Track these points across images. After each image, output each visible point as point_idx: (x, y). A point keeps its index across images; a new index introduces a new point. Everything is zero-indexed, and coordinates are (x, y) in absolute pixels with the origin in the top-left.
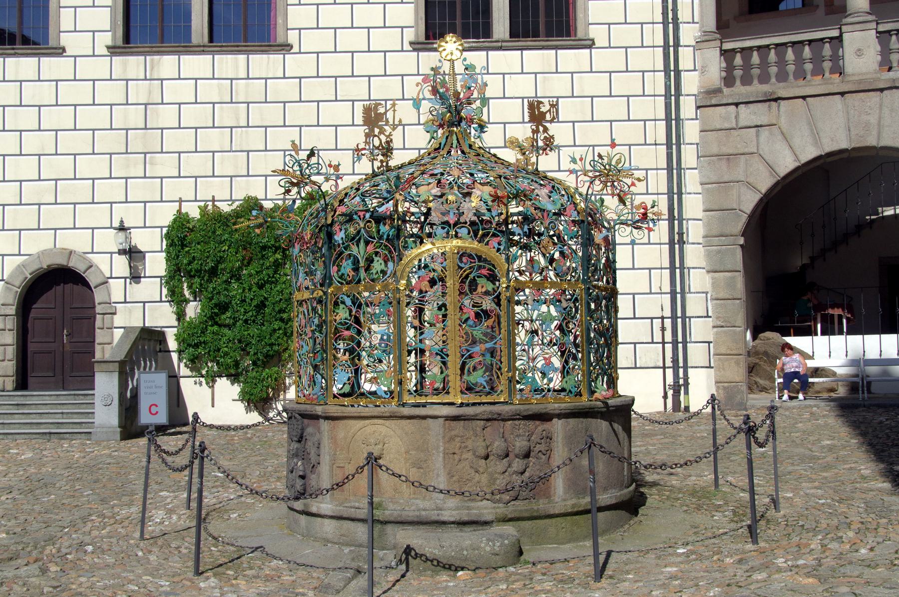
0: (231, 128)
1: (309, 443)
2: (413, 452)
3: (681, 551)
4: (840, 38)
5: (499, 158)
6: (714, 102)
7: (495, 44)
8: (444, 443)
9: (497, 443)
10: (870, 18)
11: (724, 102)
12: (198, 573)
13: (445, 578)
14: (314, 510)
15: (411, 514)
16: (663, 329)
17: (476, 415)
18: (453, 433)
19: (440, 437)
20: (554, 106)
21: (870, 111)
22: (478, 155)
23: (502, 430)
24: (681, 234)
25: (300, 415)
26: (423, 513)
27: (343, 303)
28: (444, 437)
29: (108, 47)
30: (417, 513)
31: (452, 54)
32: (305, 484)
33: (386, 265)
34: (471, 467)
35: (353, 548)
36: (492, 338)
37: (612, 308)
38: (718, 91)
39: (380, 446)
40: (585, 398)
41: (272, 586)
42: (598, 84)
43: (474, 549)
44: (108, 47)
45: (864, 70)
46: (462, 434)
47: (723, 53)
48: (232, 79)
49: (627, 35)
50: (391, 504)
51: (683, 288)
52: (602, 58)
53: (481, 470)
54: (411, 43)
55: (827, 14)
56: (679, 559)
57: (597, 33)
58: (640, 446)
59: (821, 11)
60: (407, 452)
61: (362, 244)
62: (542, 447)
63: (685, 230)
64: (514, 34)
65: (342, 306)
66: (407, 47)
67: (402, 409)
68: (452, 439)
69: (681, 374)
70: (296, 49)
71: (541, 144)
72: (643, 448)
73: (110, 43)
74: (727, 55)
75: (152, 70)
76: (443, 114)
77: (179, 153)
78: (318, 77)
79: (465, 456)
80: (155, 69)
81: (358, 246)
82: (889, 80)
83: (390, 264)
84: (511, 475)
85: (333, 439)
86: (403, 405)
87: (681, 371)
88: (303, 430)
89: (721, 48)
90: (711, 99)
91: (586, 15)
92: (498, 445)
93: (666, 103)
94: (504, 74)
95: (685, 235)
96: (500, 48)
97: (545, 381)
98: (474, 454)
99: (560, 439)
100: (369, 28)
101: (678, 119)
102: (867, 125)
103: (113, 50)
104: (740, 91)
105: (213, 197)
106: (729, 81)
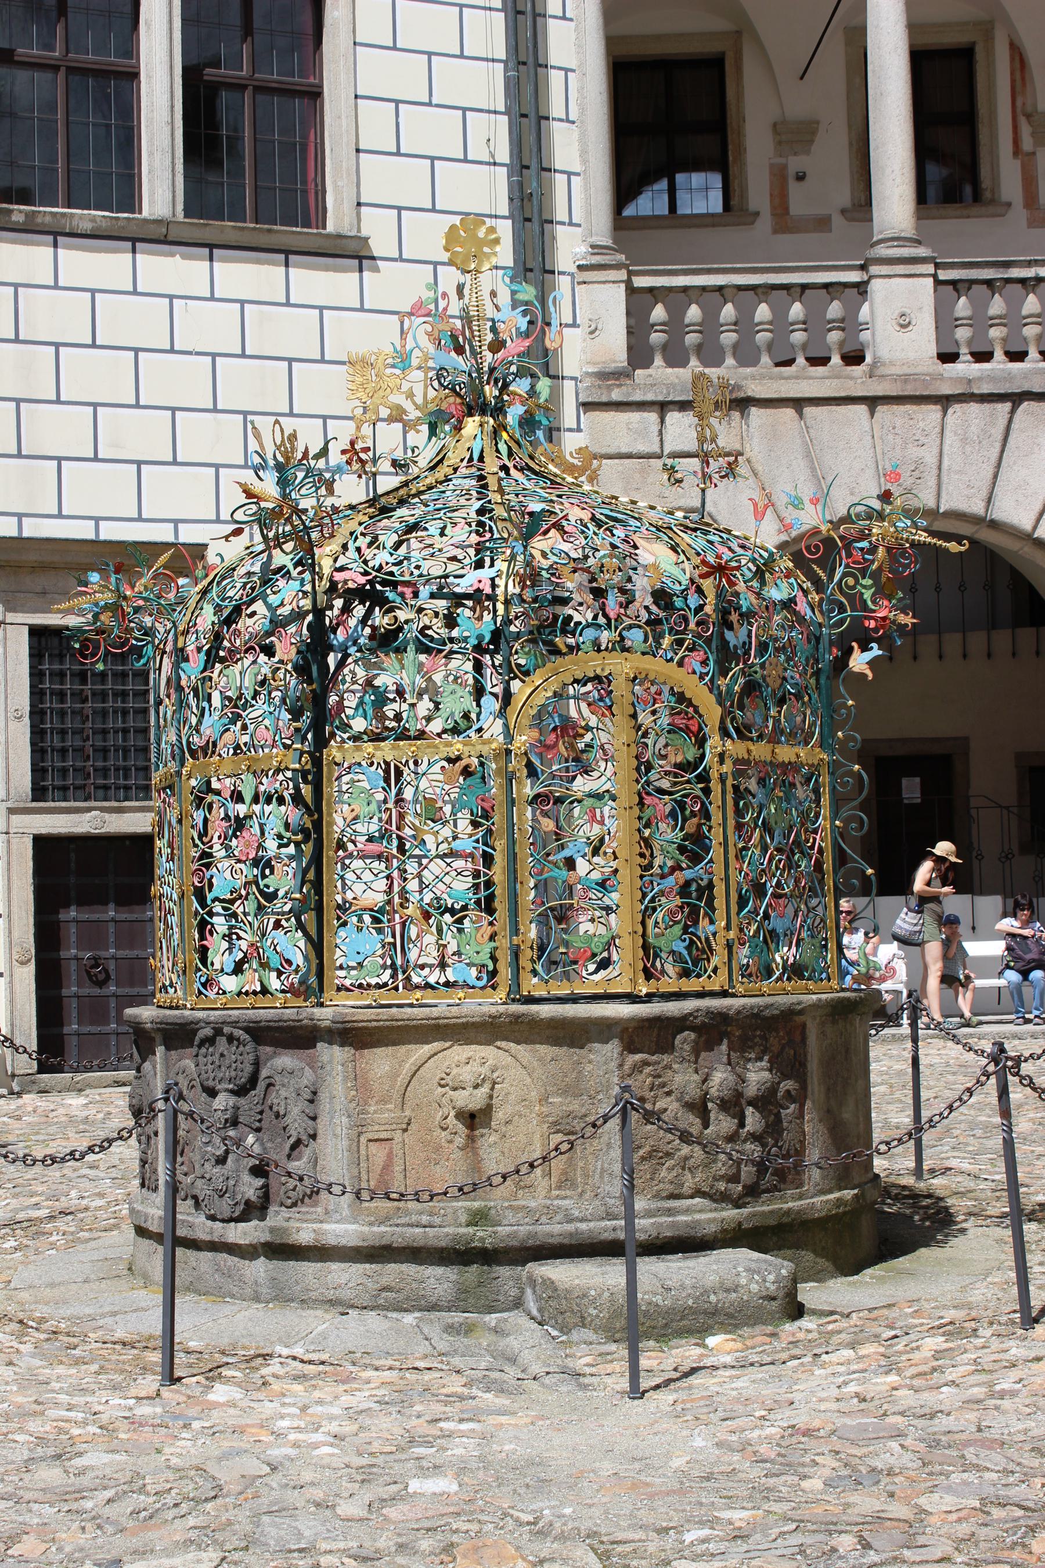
2: (557, 1100)
4: (861, 289)
6: (616, 395)
10: (922, 251)
11: (638, 397)
14: (304, 1236)
15: (557, 1229)
19: (613, 1065)
21: (923, 440)
25: (247, 1030)
26: (583, 1226)
30: (570, 1227)
32: (266, 1186)
36: (695, 859)
38: (618, 375)
39: (485, 1090)
43: (728, 1291)
45: (912, 355)
47: (631, 291)
50: (509, 1214)
55: (775, 232)
59: (765, 223)
60: (543, 1100)
64: (197, 203)
68: (638, 1068)
74: (638, 301)
82: (959, 380)
85: (359, 1082)
88: (257, 1065)
89: (628, 283)
90: (609, 388)
94: (171, 297)
96: (164, 241)
102: (918, 465)
104: (661, 377)
106: (639, 354)
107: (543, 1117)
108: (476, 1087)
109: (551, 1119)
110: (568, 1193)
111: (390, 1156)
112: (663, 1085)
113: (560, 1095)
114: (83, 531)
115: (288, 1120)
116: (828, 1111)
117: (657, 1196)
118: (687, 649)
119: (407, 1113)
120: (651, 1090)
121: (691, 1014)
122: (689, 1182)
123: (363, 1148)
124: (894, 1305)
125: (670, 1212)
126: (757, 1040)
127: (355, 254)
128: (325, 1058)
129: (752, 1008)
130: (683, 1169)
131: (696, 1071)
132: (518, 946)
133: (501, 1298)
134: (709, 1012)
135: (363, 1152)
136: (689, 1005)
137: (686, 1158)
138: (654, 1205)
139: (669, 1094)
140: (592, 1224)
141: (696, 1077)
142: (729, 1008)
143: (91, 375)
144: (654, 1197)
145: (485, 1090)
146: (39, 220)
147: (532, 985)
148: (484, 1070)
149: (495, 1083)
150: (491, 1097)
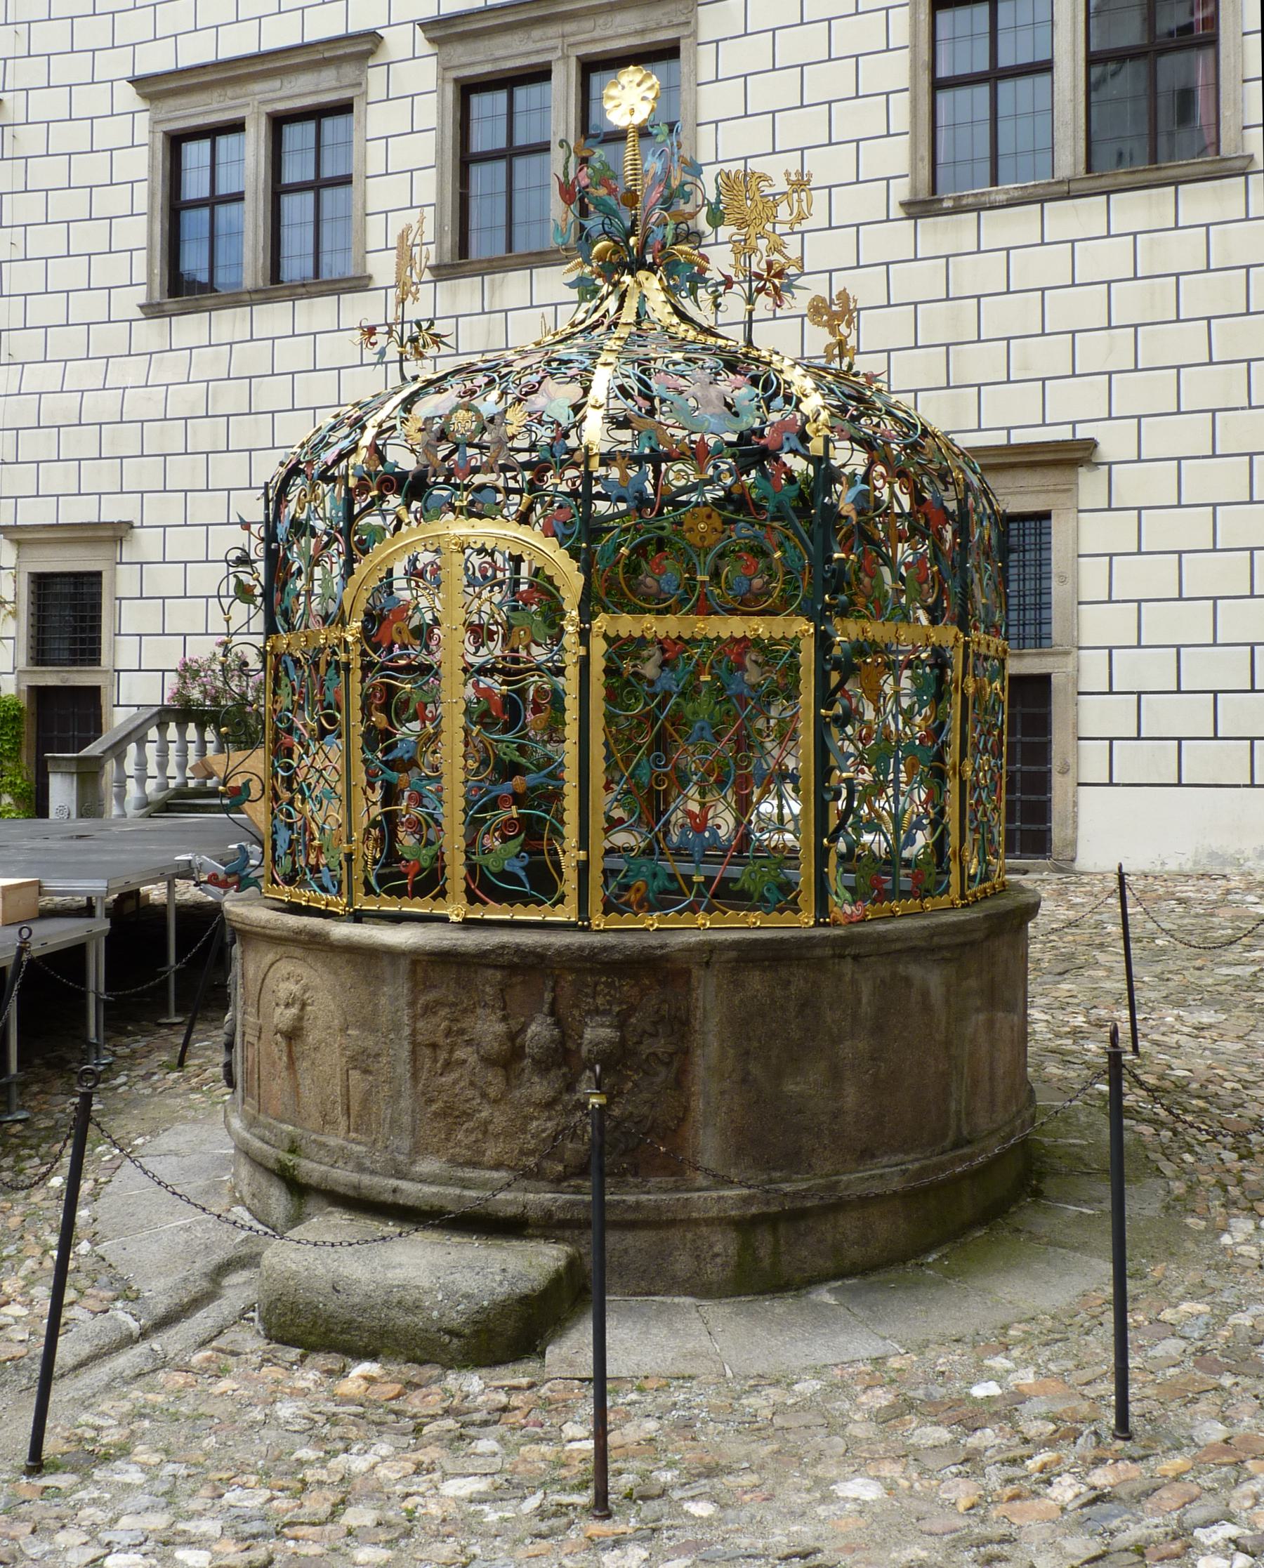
7: (1056, 188)
8: (414, 1018)
9: (533, 1028)
12: (602, 1508)
19: (403, 1002)
28: (412, 1004)
29: (141, 307)
30: (355, 1177)
39: (294, 1011)
40: (807, 918)
44: (141, 307)
46: (451, 998)
54: (902, 204)
60: (344, 1030)
62: (660, 1046)
66: (896, 212)
68: (429, 1010)
73: (143, 301)
75: (492, 296)
79: (460, 1054)
80: (497, 294)
96: (1068, 196)
99: (713, 1025)
103: (152, 310)
108: (287, 1005)
110: (363, 1138)
112: (462, 1032)
113: (358, 1028)
114: (999, 439)
116: (744, 1081)
120: (447, 1036)
121: (492, 951)
122: (492, 1151)
124: (691, 1378)
125: (465, 1184)
130: (485, 1132)
131: (504, 1019)
134: (518, 950)
137: (486, 1123)
140: (376, 1179)
142: (547, 947)
143: (1003, 315)
145: (294, 1011)
146: (964, 202)
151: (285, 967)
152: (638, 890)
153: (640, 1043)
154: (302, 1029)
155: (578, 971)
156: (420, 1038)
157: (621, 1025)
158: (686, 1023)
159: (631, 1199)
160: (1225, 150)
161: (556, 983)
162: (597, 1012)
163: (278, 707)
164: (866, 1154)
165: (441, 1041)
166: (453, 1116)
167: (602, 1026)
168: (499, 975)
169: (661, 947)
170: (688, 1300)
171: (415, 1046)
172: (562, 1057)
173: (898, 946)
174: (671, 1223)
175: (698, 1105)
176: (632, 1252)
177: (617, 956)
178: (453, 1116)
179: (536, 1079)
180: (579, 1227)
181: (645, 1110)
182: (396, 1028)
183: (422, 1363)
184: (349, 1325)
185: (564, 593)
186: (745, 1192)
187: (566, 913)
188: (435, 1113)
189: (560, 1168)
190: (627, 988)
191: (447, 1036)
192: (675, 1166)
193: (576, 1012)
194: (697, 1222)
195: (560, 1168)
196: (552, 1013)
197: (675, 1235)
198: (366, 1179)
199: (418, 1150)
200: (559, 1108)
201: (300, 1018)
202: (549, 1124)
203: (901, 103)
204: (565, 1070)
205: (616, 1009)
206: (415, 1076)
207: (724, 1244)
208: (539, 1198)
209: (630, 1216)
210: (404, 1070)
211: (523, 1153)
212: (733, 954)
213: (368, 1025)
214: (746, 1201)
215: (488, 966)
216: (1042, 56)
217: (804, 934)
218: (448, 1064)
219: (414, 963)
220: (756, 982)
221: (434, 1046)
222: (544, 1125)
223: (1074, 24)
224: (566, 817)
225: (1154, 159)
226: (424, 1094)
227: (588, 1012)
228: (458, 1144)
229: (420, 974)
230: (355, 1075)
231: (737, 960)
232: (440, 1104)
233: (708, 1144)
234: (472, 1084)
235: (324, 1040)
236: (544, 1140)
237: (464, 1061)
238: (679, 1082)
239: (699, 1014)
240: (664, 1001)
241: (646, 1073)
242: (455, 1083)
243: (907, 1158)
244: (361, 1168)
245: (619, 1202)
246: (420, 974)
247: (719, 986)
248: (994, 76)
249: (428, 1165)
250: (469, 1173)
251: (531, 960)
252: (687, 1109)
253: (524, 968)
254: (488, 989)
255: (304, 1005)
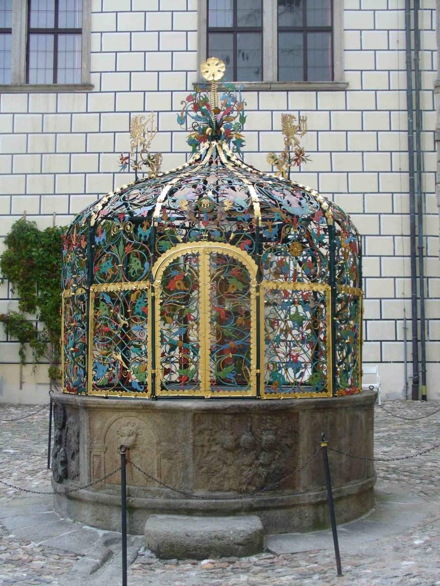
0: (41, 154)
1: (70, 432)
2: (164, 444)
3: (417, 542)
5: (254, 169)
7: (265, 86)
8: (194, 436)
13: (189, 566)
16: (405, 329)
17: (226, 409)
18: (202, 427)
20: (302, 120)
22: (236, 165)
23: (249, 424)
24: (421, 249)
27: (103, 300)
28: (193, 431)
30: (167, 501)
31: (213, 75)
33: (143, 266)
34: (219, 459)
35: (107, 532)
37: (358, 311)
39: (132, 438)
41: (21, 573)
42: (351, 120)
48: (43, 114)
49: (376, 80)
51: (422, 295)
52: (356, 100)
53: (229, 462)
54: (193, 84)
56: (416, 551)
57: (352, 79)
58: (383, 431)
60: (158, 443)
61: (121, 246)
62: (289, 441)
63: (424, 245)
65: (102, 303)
67: (153, 402)
68: (201, 432)
69: (420, 369)
70: (97, 89)
71: (293, 155)
72: (386, 434)
76: (205, 129)
77: (69, 195)
78: (115, 112)
81: (117, 246)
83: (147, 264)
84: (257, 467)
86: (157, 398)
87: (420, 365)
91: (342, 63)
92: (246, 438)
93: (409, 138)
95: (424, 250)
97: (298, 375)
98: (222, 447)
100: (158, 72)
101: (423, 319)
105: (25, 211)
107: (158, 451)
108: (129, 436)
109: (161, 452)
111: (100, 462)
115: (71, 443)
117: (211, 490)
118: (243, 239)
119: (106, 444)
120: (208, 442)
122: (226, 485)
123: (92, 458)
126: (268, 420)
127: (344, 88)
128: (81, 419)
129: (263, 406)
130: (224, 478)
132: (155, 374)
133: (140, 528)
134: (239, 407)
135: (92, 460)
136: (229, 403)
138: (209, 494)
139: (217, 444)
141: (231, 437)
142: (250, 406)
144: (209, 490)
145: (132, 438)
147: (159, 393)
148: (133, 429)
149: (137, 435)
150: (136, 440)
151: (124, 421)
152: (276, 384)
153: (281, 440)
154: (136, 445)
155: (259, 414)
156: (196, 444)
157: (276, 434)
158: (296, 432)
159: (280, 498)
160: (336, 79)
161: (252, 419)
162: (267, 430)
163: (98, 314)
164: (348, 480)
165: (206, 444)
166: (211, 473)
167: (269, 434)
168: (230, 417)
169: (292, 404)
170: (298, 534)
171: (194, 446)
172: (255, 447)
173: (358, 404)
174: (294, 506)
175: (301, 463)
176: (279, 518)
177: (277, 408)
178: (211, 473)
179: (245, 455)
180: (261, 510)
181: (283, 465)
182: (185, 440)
183: (228, 557)
184: (195, 549)
185: (250, 272)
186: (316, 493)
187: (252, 393)
188: (203, 472)
189: (254, 488)
190: (278, 421)
191: (208, 442)
192: (291, 485)
193: (259, 430)
194: (300, 505)
195: (254, 488)
196: (251, 431)
197: (293, 510)
198: (172, 501)
199: (196, 487)
200: (253, 466)
201: (136, 440)
202: (250, 472)
203: (193, 37)
204: (255, 452)
205: (274, 428)
206: (194, 459)
207: (308, 512)
208: (248, 500)
209: (280, 504)
210: (189, 456)
211: (240, 484)
212: (313, 406)
213: (171, 440)
214: (317, 496)
215: (226, 414)
216: (282, 35)
217: (329, 399)
218: (208, 452)
219: (195, 414)
220: (318, 416)
221: (203, 446)
222: (248, 472)
223: (273, 13)
224: (252, 357)
225: (305, 78)
226: (198, 465)
227: (264, 430)
228: (213, 483)
229: (197, 418)
230: (164, 461)
231: (315, 409)
232: (206, 468)
233: (304, 477)
234: (219, 459)
235: (148, 449)
236: (249, 478)
237: (216, 451)
238: (294, 455)
239: (301, 429)
240: (290, 425)
241: (283, 452)
242: (212, 459)
243: (358, 481)
244: (168, 497)
245: (276, 499)
246: (197, 418)
247: (307, 419)
248: (56, 32)
249: (200, 493)
250: (218, 494)
251: (244, 411)
252: (297, 464)
253: (240, 414)
254: (226, 423)
255: (137, 435)
